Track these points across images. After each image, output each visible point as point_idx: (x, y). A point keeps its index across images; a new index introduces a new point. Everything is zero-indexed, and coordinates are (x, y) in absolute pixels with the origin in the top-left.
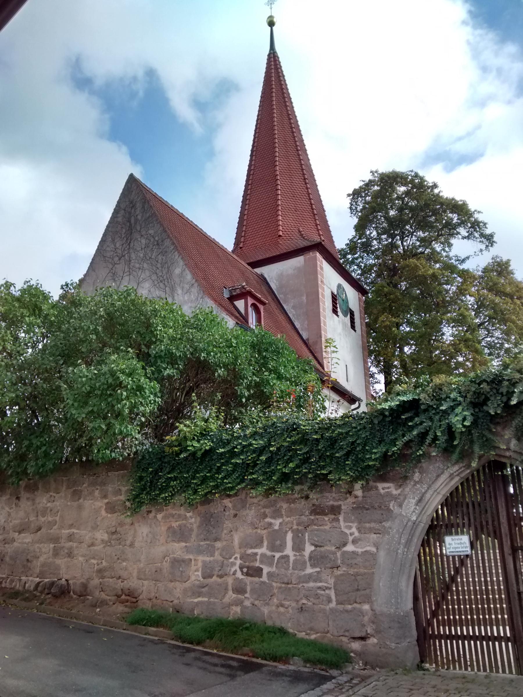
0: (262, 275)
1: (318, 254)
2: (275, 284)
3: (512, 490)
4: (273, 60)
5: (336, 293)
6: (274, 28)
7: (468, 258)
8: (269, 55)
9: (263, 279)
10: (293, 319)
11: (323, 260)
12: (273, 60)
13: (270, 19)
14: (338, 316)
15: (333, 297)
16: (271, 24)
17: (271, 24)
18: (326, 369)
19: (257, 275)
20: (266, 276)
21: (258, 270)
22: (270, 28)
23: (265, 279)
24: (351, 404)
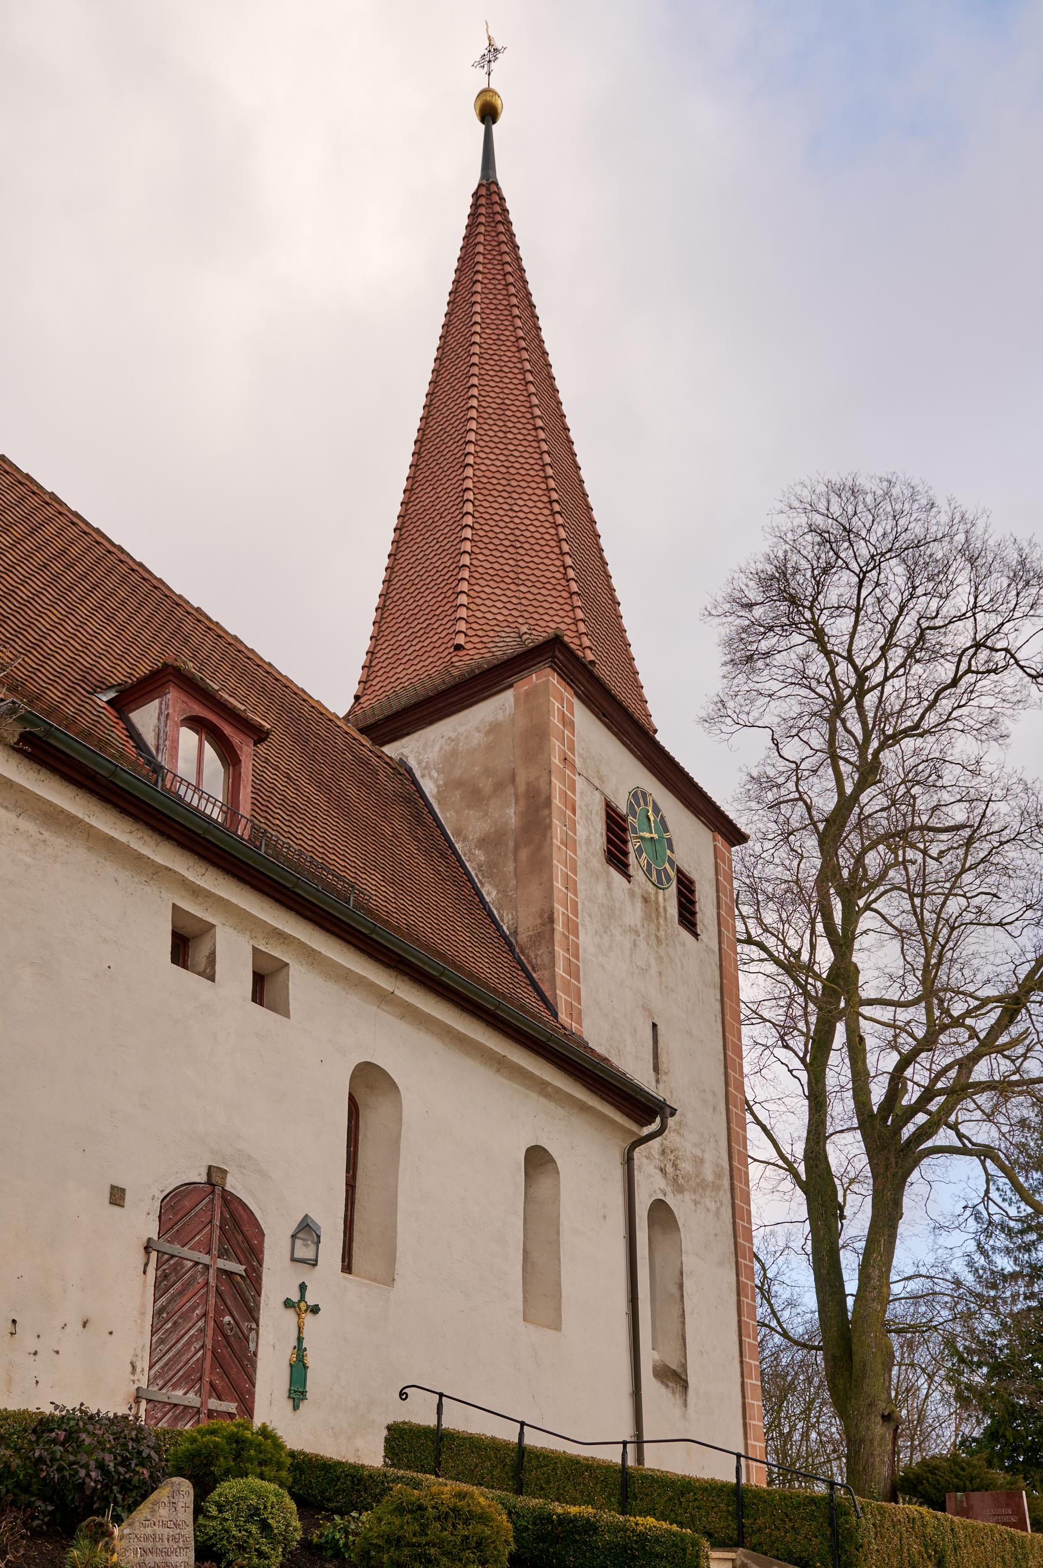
0: (402, 763)
1: (554, 680)
2: (435, 781)
3: (842, 1005)
4: (488, 207)
5: (623, 809)
6: (495, 128)
7: (489, 38)
8: (476, 195)
9: (403, 771)
10: (728, 1173)
11: (575, 701)
12: (488, 207)
13: (483, 98)
14: (628, 877)
15: (609, 816)
16: (488, 113)
17: (488, 113)
18: (563, 1016)
19: (388, 762)
20: (412, 763)
21: (391, 750)
22: (483, 127)
23: (410, 771)
24: (642, 1125)
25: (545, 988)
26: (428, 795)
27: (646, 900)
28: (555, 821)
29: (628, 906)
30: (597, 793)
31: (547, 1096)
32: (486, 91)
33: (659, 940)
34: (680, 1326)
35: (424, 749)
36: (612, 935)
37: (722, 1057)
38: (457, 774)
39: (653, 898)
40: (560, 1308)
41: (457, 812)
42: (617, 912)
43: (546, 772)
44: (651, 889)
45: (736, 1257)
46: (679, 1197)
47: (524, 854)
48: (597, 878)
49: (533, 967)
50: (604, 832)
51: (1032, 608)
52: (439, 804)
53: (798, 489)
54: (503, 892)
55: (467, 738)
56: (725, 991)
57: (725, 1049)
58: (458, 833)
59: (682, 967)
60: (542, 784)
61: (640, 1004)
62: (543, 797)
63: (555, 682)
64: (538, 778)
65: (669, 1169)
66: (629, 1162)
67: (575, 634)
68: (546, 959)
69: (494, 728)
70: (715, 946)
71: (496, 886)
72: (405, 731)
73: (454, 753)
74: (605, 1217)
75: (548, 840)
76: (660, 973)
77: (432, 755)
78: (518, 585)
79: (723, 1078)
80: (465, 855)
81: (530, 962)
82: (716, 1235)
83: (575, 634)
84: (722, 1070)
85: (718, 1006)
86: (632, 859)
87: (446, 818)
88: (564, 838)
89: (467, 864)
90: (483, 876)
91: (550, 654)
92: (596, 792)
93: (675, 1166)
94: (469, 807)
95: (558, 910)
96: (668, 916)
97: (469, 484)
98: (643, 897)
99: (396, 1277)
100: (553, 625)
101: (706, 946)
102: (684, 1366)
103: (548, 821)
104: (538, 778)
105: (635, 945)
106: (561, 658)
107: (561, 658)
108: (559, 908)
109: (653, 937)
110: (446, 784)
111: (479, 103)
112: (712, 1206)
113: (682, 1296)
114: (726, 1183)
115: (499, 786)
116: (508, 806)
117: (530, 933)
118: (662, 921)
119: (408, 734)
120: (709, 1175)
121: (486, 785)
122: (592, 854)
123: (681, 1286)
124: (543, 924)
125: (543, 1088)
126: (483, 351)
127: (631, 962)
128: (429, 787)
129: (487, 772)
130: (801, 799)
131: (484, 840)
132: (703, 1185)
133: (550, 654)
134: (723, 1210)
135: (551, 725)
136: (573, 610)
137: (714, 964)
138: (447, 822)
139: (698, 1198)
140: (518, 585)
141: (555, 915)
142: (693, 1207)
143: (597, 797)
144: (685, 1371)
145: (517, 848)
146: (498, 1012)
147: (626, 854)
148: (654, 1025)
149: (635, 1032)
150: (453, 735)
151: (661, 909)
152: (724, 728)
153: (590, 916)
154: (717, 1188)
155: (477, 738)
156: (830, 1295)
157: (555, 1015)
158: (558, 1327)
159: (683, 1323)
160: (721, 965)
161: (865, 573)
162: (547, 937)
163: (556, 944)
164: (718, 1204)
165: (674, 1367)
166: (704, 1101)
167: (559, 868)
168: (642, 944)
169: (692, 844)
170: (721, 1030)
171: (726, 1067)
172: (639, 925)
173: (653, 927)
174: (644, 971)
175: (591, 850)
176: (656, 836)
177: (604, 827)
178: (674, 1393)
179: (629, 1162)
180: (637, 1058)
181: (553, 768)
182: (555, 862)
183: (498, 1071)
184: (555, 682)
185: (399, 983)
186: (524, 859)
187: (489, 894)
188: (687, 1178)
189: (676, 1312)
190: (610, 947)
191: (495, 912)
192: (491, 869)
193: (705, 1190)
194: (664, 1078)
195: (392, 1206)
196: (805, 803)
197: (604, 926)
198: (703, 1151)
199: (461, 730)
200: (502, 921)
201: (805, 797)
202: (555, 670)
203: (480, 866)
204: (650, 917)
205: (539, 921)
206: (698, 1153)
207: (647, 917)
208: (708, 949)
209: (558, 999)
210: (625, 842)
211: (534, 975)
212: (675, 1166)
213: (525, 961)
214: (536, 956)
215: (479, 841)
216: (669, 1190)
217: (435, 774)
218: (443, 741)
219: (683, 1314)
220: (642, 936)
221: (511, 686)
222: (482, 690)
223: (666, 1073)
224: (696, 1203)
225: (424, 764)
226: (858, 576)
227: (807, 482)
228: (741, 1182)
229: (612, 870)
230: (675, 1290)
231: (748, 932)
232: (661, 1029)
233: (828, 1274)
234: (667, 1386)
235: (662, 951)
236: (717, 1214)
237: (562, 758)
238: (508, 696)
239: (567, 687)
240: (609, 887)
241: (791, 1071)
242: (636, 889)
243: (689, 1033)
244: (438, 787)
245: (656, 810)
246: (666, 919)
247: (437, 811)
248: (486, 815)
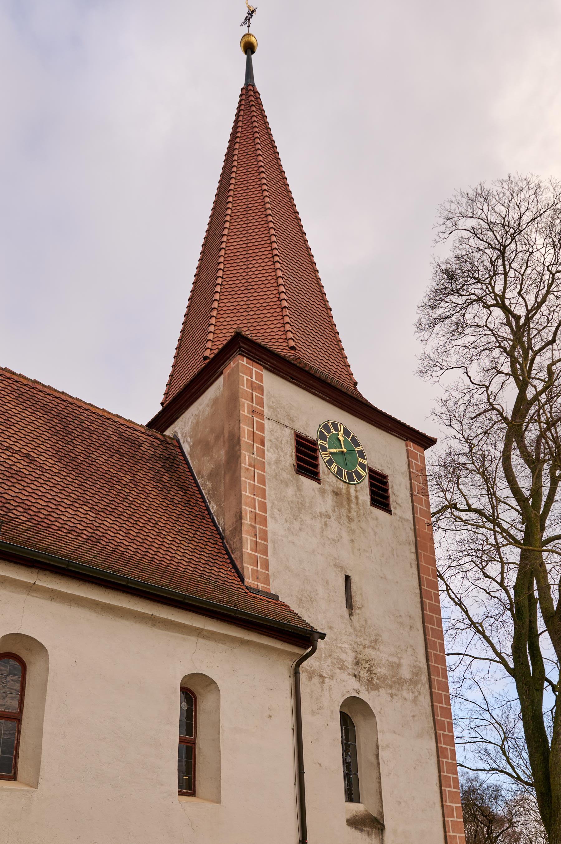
2: (189, 443)
4: (250, 99)
10: (426, 671)
12: (250, 99)
16: (249, 48)
17: (249, 48)
21: (168, 433)
25: (237, 563)
26: (186, 453)
27: (336, 493)
28: (243, 452)
29: (319, 499)
30: (287, 431)
31: (205, 637)
32: (248, 35)
33: (350, 519)
34: (378, 785)
35: (185, 426)
36: (302, 521)
37: (418, 591)
38: (199, 436)
39: (344, 491)
40: (220, 787)
41: (198, 460)
42: (308, 505)
43: (238, 422)
44: (341, 485)
45: (435, 730)
46: (374, 693)
47: (228, 478)
48: (287, 484)
49: (232, 551)
50: (294, 454)
51: (452, 202)
52: (191, 457)
53: (447, 205)
54: (219, 505)
55: (203, 412)
56: (419, 545)
57: (420, 585)
58: (199, 473)
59: (375, 534)
60: (236, 431)
61: (332, 564)
62: (236, 438)
63: (245, 363)
64: (234, 427)
65: (364, 674)
66: (296, 674)
67: (283, 333)
68: (238, 544)
69: (216, 401)
70: (409, 515)
71: (216, 503)
72: (175, 417)
73: (197, 423)
74: (270, 717)
75: (239, 465)
76: (352, 541)
77: (188, 428)
78: (248, 312)
79: (419, 606)
80: (202, 486)
81: (231, 548)
82: (413, 716)
83: (283, 333)
84: (418, 599)
85: (413, 556)
86: (322, 467)
87: (194, 465)
88: (253, 462)
89: (203, 492)
90: (210, 497)
91: (238, 346)
92: (286, 429)
93: (370, 671)
94: (204, 455)
95: (246, 510)
96: (360, 501)
97: (222, 259)
98: (334, 492)
99: (40, 781)
100: (235, 326)
101: (400, 517)
102: (381, 814)
103: (238, 453)
104: (234, 427)
105: (326, 524)
106: (244, 346)
107: (244, 346)
108: (247, 509)
109: (344, 518)
110: (194, 444)
111: (242, 45)
112: (410, 696)
113: (378, 764)
114: (424, 678)
115: (217, 438)
116: (221, 449)
117: (231, 529)
118: (353, 506)
119: (177, 418)
120: (406, 673)
121: (211, 439)
122: (282, 469)
123: (377, 756)
124: (237, 521)
125: (199, 633)
126: (237, 181)
127: (322, 536)
128: (186, 448)
129: (212, 431)
130: (494, 409)
131: (211, 474)
132: (400, 682)
133: (238, 346)
134: (421, 698)
135: (241, 391)
136: (283, 318)
137: (408, 530)
138: (194, 468)
139: (394, 691)
140: (248, 312)
141: (243, 514)
142: (389, 699)
143: (293, 432)
144: (382, 817)
145: (225, 473)
146: (129, 585)
147: (316, 466)
148: (347, 578)
149: (327, 583)
150: (197, 413)
151: (353, 498)
152: (434, 374)
153: (280, 510)
154: (414, 682)
155: (208, 410)
156: (535, 748)
157: (243, 580)
158: (218, 801)
159: (380, 783)
160: (415, 529)
161: (505, 247)
162: (239, 530)
163: (243, 532)
164: (416, 694)
165: (375, 815)
166: (401, 623)
167: (246, 482)
168: (333, 523)
169: (383, 452)
170: (416, 572)
171: (421, 598)
172: (330, 512)
173: (344, 511)
174: (335, 542)
175: (281, 467)
176: (344, 450)
177: (294, 450)
178: (369, 835)
179: (296, 674)
180: (329, 601)
181: (241, 419)
182: (243, 479)
183: (154, 625)
184: (245, 363)
185: (41, 576)
186: (228, 481)
187: (213, 508)
188: (383, 678)
189: (375, 775)
190: (300, 529)
191: (216, 519)
192: (214, 491)
193: (402, 685)
194: (358, 611)
195: (40, 730)
196: (498, 411)
197: (294, 516)
198: (400, 658)
199: (200, 408)
200: (219, 523)
201: (496, 406)
202: (244, 356)
203: (209, 491)
204: (342, 504)
205: (235, 520)
206: (396, 660)
207: (339, 505)
208: (401, 519)
209: (245, 570)
210: (316, 458)
211: (233, 556)
212: (370, 671)
213: (228, 548)
214: (233, 543)
215: (208, 476)
216: (363, 689)
217: (189, 439)
218: (192, 418)
219: (380, 776)
220: (333, 518)
221: (221, 373)
222: (207, 380)
223: (359, 608)
224: (392, 695)
225: (184, 435)
226: (499, 250)
227: (453, 199)
228: (438, 676)
229: (301, 477)
230: (373, 759)
231: (468, 504)
232: (354, 579)
233: (533, 733)
234: (361, 830)
235: (354, 526)
236: (415, 701)
237: (251, 410)
238: (221, 379)
239: (254, 363)
240: (299, 489)
241: (489, 593)
242: (327, 487)
243: (384, 578)
244: (190, 447)
245: (347, 433)
246: (357, 504)
247: (190, 462)
248: (211, 458)
